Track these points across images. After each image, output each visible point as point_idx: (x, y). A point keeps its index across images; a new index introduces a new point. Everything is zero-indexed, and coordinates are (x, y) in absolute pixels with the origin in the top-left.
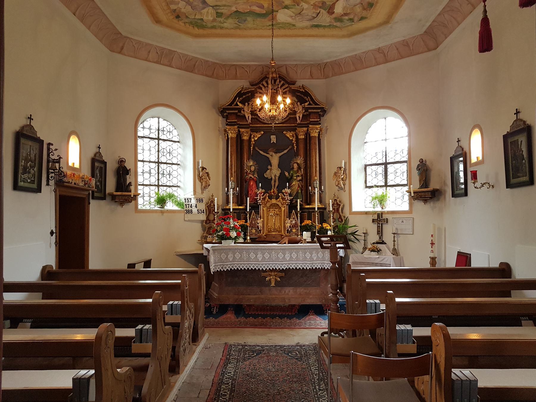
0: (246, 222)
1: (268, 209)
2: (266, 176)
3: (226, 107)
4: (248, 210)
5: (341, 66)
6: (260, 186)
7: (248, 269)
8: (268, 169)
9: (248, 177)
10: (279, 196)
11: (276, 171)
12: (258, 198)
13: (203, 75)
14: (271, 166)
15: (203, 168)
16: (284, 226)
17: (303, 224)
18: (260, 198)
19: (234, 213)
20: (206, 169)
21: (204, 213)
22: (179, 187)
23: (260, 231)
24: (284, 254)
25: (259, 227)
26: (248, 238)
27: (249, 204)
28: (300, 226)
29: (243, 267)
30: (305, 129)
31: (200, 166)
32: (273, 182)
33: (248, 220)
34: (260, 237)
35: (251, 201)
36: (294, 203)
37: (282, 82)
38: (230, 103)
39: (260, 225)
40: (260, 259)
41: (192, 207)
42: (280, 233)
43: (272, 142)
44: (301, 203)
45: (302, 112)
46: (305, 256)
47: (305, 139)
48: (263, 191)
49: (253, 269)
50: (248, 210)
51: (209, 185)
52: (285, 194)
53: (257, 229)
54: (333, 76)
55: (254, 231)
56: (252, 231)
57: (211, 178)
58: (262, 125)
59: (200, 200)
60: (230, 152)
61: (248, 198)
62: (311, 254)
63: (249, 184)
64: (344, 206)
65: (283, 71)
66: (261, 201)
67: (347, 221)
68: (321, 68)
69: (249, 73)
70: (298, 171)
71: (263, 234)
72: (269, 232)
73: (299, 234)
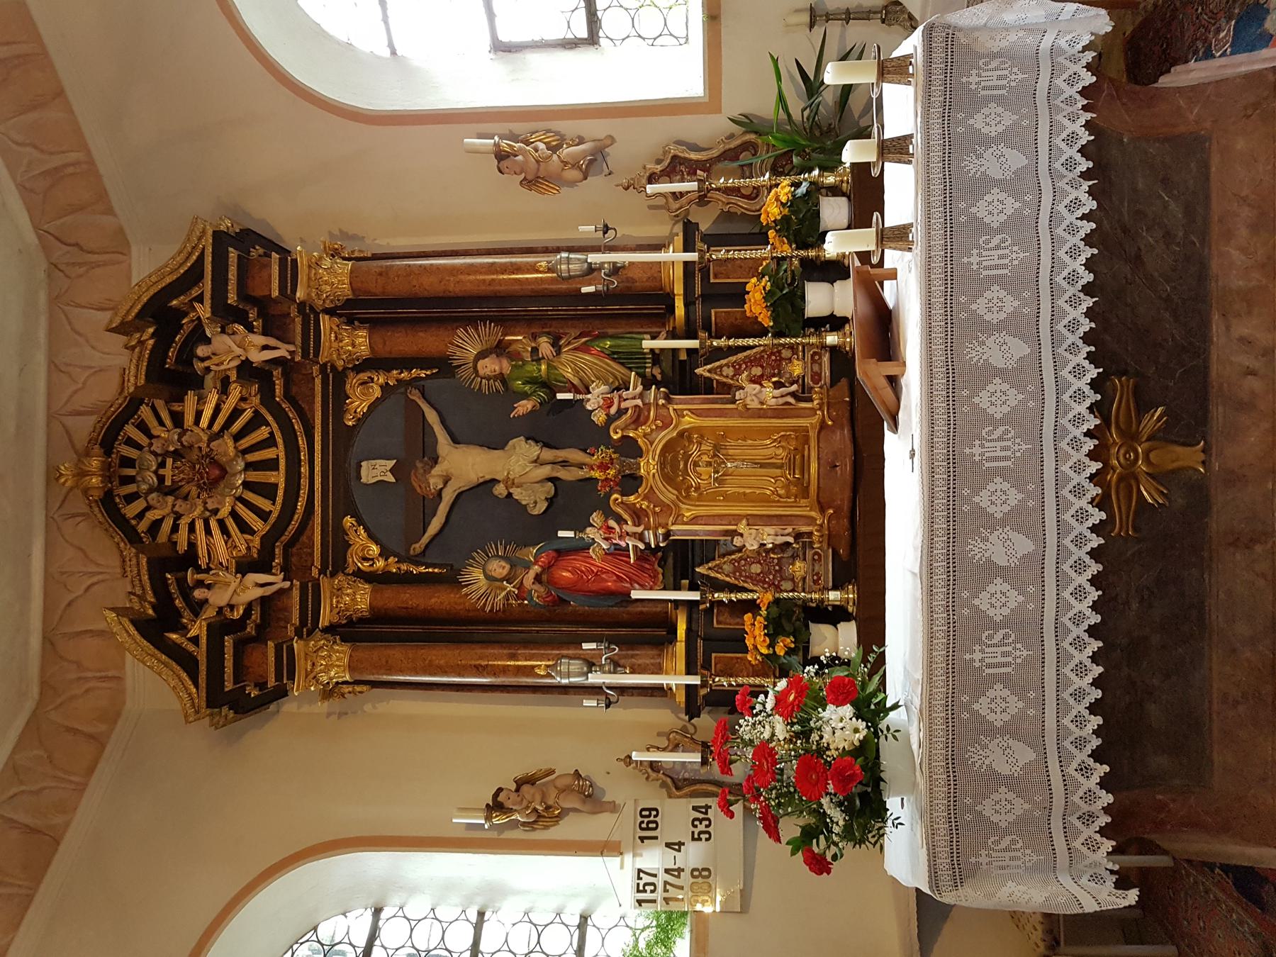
0: (752, 606)
1: (688, 496)
2: (542, 506)
3: (204, 694)
4: (695, 596)
5: (56, 169)
6: (570, 534)
7: (1093, 631)
8: (510, 495)
9: (538, 593)
10: (623, 437)
11: (514, 458)
12: (635, 547)
13: (81, 789)
14: (494, 481)
15: (496, 806)
16: (778, 413)
17: (766, 321)
18: (634, 535)
19: (707, 665)
20: (500, 790)
21: (707, 807)
22: (584, 919)
23: (798, 536)
24: (988, 373)
25: (780, 540)
26: (834, 596)
27: (664, 589)
28: (778, 334)
29: (1080, 670)
30: (325, 322)
31: (483, 822)
32: (565, 474)
33: (744, 596)
34: (831, 539)
35: (649, 583)
36: (662, 373)
37: (131, 430)
38: (184, 675)
39: (769, 536)
40: (1024, 545)
41: (680, 870)
42: (813, 435)
43: (390, 478)
44: (664, 334)
45: (238, 338)
46: (999, 231)
47: (373, 324)
48: (596, 518)
49: (1094, 594)
50: (695, 596)
51: (577, 775)
52: (613, 410)
53: (789, 553)
54: (110, 211)
55: (799, 568)
56: (799, 575)
57: (544, 767)
58: (318, 519)
59: (648, 824)
60: (417, 674)
61: (636, 594)
62: (983, 185)
63: (573, 588)
64: (679, 143)
65: (85, 427)
66: (647, 528)
67: (747, 123)
68: (80, 265)
69: (100, 577)
70: (514, 357)
71: (814, 521)
72: (805, 493)
73: (813, 340)
